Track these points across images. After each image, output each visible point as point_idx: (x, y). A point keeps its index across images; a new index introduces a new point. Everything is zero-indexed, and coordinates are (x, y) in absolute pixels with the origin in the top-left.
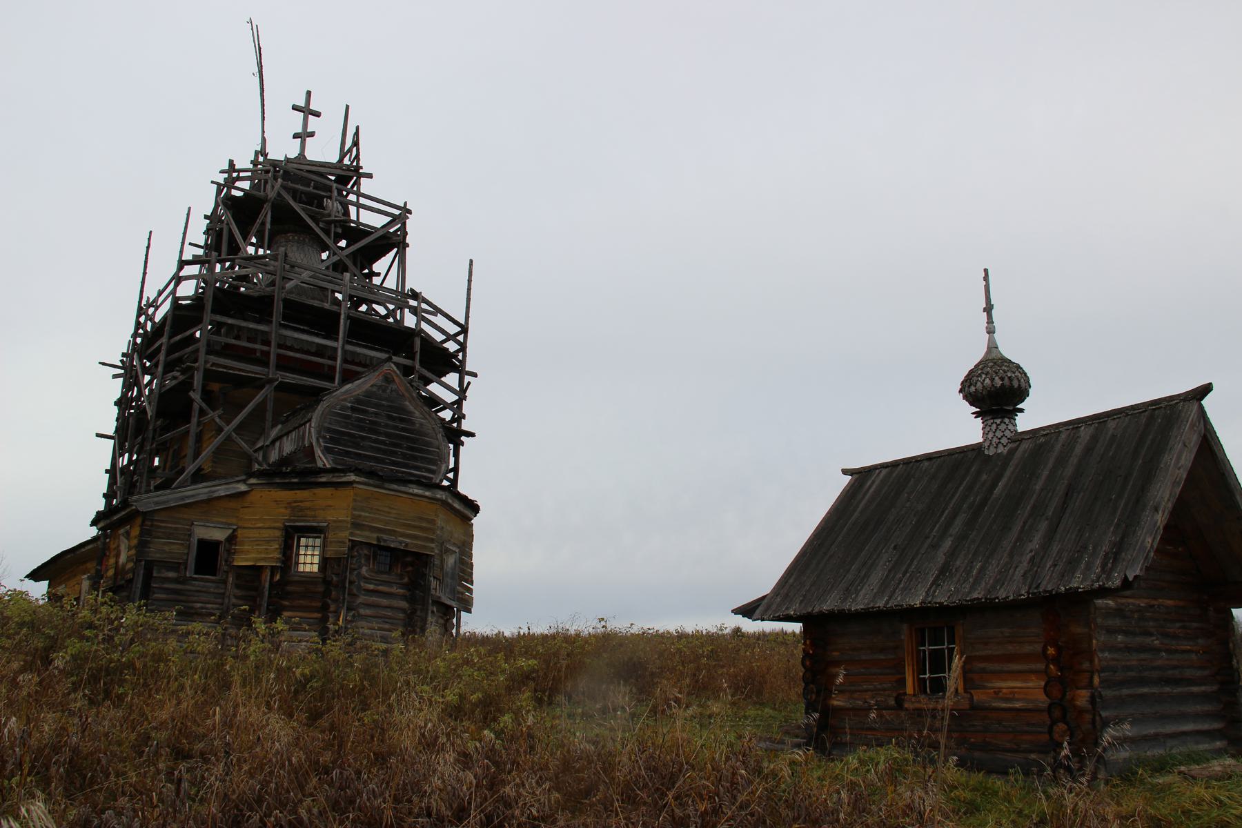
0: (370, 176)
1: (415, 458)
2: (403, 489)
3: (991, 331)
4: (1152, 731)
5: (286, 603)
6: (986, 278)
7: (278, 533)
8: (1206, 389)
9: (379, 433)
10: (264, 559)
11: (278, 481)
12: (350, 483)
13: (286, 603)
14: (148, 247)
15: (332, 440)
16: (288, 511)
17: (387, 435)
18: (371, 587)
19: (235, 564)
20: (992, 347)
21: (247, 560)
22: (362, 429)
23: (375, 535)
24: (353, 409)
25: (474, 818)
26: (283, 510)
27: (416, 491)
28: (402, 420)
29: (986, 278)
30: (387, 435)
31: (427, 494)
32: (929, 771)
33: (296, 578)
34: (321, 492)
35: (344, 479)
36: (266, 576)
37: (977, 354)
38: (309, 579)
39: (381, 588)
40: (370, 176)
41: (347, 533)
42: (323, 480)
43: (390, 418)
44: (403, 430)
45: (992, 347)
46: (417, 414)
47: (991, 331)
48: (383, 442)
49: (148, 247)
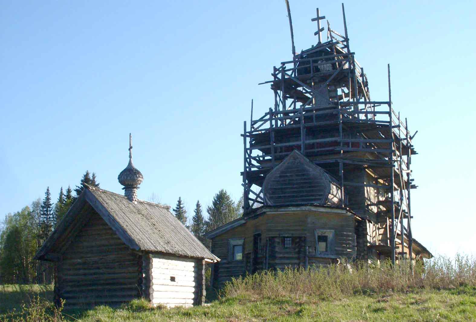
2: (286, 209)
3: (130, 157)
4: (204, 282)
9: (294, 184)
15: (273, 193)
18: (281, 255)
20: (130, 163)
22: (286, 184)
23: (278, 233)
24: (280, 177)
27: (293, 209)
28: (303, 175)
31: (299, 209)
37: (125, 166)
38: (239, 262)
39: (286, 255)
43: (297, 175)
44: (305, 179)
45: (130, 163)
46: (311, 169)
47: (130, 157)
48: (296, 188)
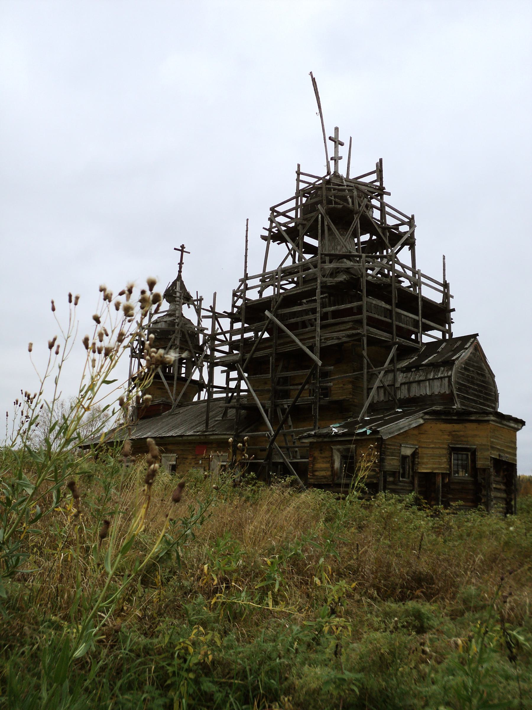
0: (389, 194)
1: (487, 400)
5: (450, 496)
6: (444, 259)
7: (445, 452)
8: (477, 335)
10: (436, 469)
11: (444, 418)
12: (488, 421)
13: (450, 496)
14: (247, 231)
16: (450, 438)
17: (478, 385)
19: (419, 471)
21: (427, 469)
25: (530, 635)
26: (447, 437)
29: (444, 259)
30: (478, 385)
32: (335, 590)
33: (456, 481)
34: (468, 425)
35: (486, 418)
36: (439, 480)
40: (389, 194)
41: (488, 453)
42: (473, 418)
49: (247, 231)
